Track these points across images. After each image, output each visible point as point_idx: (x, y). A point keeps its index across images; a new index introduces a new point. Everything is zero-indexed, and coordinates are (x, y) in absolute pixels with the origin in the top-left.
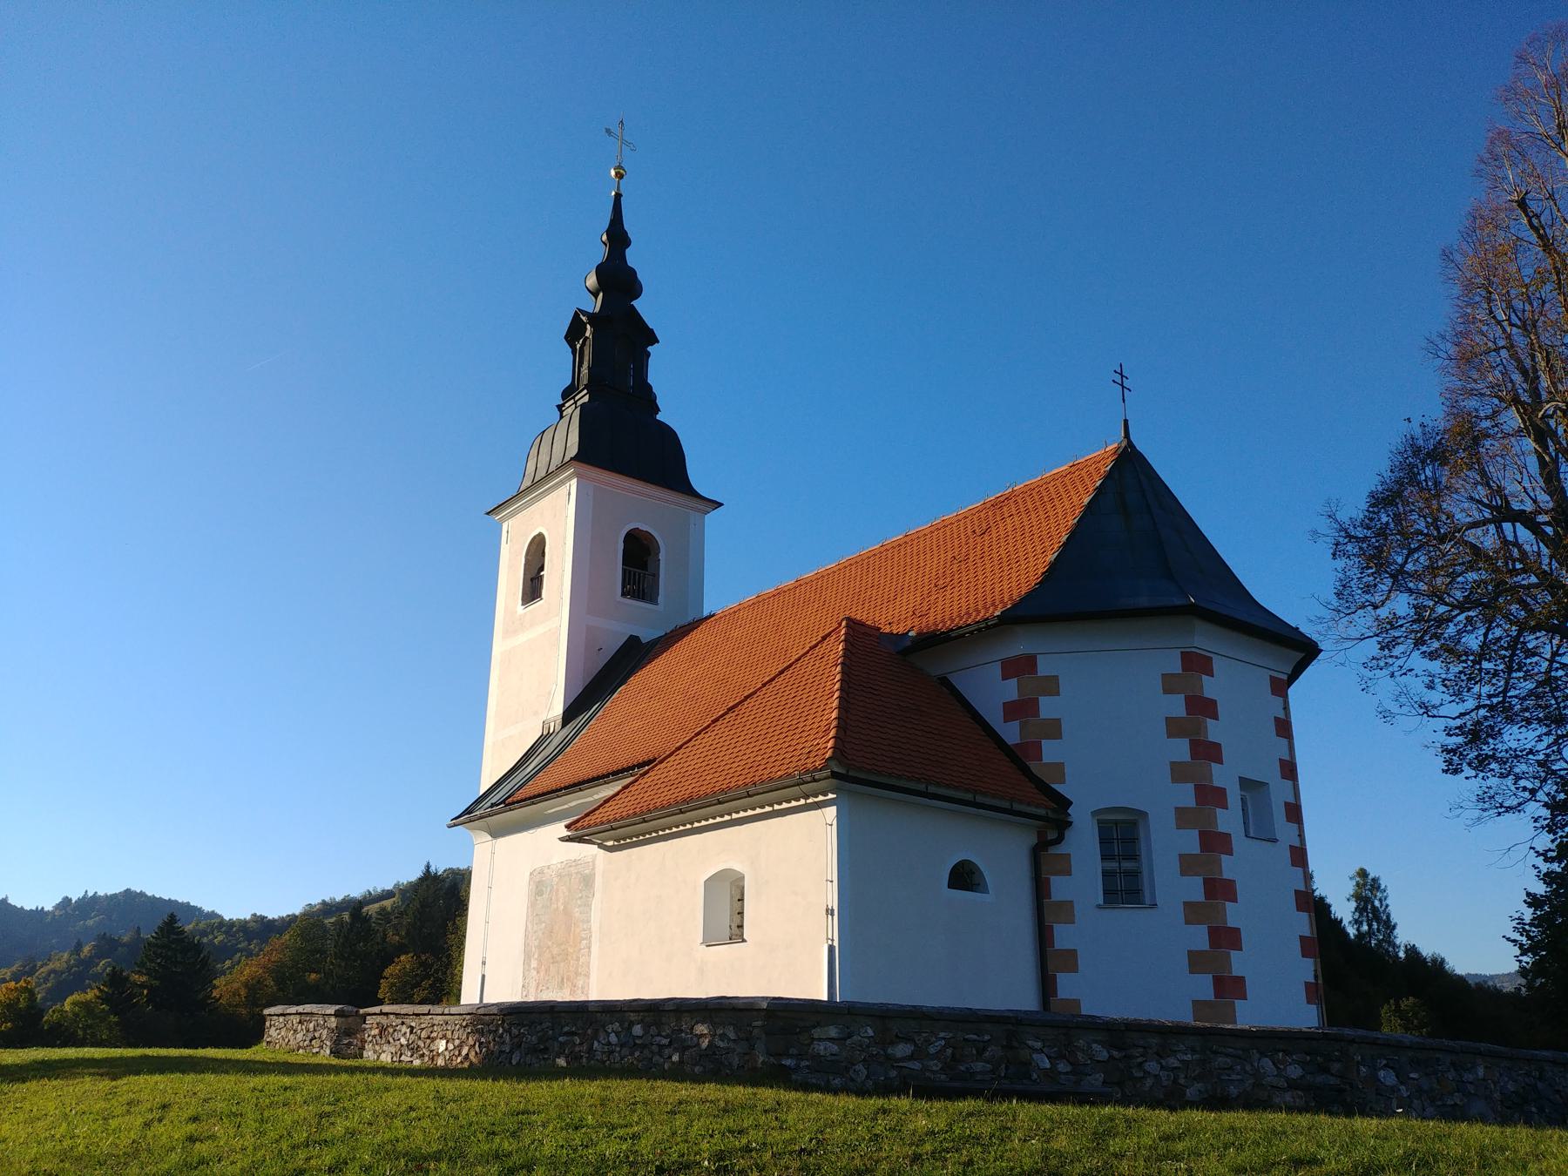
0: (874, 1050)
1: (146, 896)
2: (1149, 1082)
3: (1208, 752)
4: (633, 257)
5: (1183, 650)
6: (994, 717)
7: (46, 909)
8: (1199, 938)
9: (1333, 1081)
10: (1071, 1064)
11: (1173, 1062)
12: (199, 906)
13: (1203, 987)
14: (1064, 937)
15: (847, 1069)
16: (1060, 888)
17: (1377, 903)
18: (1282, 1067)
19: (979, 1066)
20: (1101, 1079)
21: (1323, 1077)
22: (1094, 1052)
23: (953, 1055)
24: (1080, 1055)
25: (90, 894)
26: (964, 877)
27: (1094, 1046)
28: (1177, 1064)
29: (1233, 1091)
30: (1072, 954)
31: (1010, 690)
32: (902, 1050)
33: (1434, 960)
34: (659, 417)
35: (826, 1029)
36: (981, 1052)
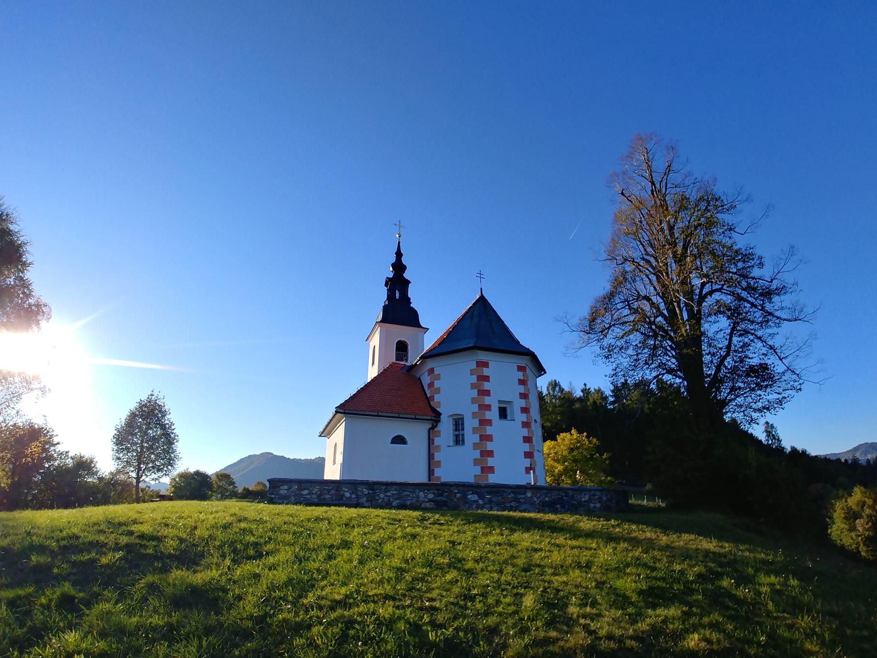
0: (297, 493)
2: (380, 500)
4: (404, 260)
5: (519, 365)
8: (477, 454)
9: (444, 499)
11: (389, 494)
13: (477, 470)
14: (437, 457)
16: (437, 441)
17: (774, 433)
19: (327, 496)
26: (399, 440)
27: (364, 490)
28: (390, 495)
29: (408, 503)
30: (439, 462)
32: (306, 492)
33: (803, 451)
34: (411, 305)
36: (329, 493)
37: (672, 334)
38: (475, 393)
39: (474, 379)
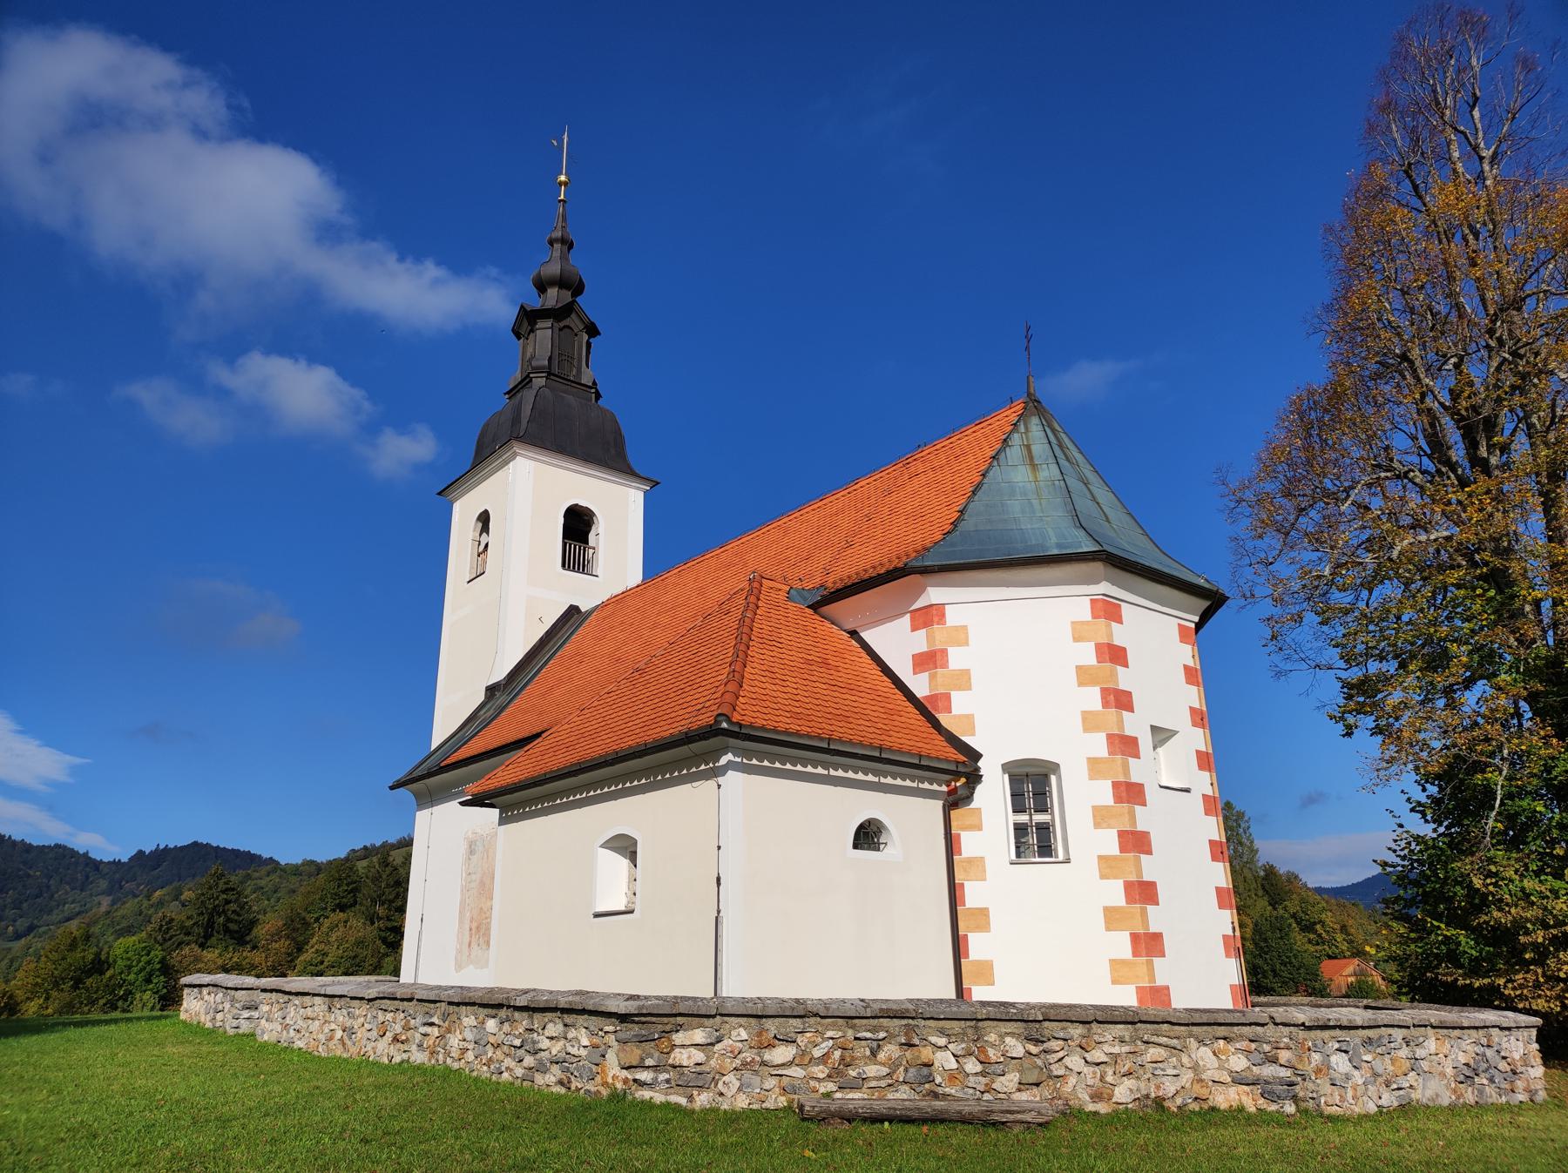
1: (212, 847)
3: (1121, 700)
6: (904, 671)
7: (122, 861)
9: (1285, 1073)
10: (981, 1063)
11: (1097, 1055)
12: (259, 853)
14: (974, 895)
15: (715, 1081)
16: (970, 844)
18: (1223, 1057)
19: (872, 1070)
20: (1016, 1080)
21: (1271, 1068)
22: (1007, 1048)
23: (842, 1059)
24: (991, 1052)
25: (161, 847)
26: (868, 836)
27: (1008, 1040)
28: (1104, 1058)
30: (983, 913)
31: (919, 642)
32: (782, 1054)
35: (691, 1032)
37: (1407, 575)
38: (1092, 698)
39: (1087, 654)
